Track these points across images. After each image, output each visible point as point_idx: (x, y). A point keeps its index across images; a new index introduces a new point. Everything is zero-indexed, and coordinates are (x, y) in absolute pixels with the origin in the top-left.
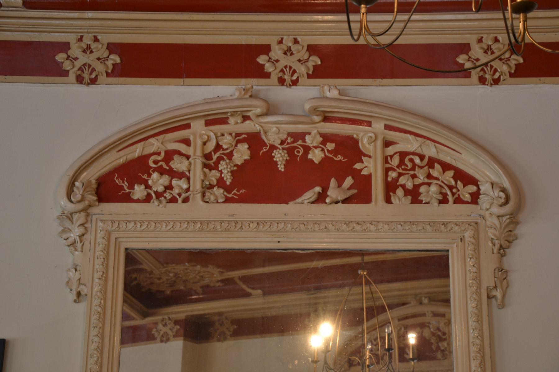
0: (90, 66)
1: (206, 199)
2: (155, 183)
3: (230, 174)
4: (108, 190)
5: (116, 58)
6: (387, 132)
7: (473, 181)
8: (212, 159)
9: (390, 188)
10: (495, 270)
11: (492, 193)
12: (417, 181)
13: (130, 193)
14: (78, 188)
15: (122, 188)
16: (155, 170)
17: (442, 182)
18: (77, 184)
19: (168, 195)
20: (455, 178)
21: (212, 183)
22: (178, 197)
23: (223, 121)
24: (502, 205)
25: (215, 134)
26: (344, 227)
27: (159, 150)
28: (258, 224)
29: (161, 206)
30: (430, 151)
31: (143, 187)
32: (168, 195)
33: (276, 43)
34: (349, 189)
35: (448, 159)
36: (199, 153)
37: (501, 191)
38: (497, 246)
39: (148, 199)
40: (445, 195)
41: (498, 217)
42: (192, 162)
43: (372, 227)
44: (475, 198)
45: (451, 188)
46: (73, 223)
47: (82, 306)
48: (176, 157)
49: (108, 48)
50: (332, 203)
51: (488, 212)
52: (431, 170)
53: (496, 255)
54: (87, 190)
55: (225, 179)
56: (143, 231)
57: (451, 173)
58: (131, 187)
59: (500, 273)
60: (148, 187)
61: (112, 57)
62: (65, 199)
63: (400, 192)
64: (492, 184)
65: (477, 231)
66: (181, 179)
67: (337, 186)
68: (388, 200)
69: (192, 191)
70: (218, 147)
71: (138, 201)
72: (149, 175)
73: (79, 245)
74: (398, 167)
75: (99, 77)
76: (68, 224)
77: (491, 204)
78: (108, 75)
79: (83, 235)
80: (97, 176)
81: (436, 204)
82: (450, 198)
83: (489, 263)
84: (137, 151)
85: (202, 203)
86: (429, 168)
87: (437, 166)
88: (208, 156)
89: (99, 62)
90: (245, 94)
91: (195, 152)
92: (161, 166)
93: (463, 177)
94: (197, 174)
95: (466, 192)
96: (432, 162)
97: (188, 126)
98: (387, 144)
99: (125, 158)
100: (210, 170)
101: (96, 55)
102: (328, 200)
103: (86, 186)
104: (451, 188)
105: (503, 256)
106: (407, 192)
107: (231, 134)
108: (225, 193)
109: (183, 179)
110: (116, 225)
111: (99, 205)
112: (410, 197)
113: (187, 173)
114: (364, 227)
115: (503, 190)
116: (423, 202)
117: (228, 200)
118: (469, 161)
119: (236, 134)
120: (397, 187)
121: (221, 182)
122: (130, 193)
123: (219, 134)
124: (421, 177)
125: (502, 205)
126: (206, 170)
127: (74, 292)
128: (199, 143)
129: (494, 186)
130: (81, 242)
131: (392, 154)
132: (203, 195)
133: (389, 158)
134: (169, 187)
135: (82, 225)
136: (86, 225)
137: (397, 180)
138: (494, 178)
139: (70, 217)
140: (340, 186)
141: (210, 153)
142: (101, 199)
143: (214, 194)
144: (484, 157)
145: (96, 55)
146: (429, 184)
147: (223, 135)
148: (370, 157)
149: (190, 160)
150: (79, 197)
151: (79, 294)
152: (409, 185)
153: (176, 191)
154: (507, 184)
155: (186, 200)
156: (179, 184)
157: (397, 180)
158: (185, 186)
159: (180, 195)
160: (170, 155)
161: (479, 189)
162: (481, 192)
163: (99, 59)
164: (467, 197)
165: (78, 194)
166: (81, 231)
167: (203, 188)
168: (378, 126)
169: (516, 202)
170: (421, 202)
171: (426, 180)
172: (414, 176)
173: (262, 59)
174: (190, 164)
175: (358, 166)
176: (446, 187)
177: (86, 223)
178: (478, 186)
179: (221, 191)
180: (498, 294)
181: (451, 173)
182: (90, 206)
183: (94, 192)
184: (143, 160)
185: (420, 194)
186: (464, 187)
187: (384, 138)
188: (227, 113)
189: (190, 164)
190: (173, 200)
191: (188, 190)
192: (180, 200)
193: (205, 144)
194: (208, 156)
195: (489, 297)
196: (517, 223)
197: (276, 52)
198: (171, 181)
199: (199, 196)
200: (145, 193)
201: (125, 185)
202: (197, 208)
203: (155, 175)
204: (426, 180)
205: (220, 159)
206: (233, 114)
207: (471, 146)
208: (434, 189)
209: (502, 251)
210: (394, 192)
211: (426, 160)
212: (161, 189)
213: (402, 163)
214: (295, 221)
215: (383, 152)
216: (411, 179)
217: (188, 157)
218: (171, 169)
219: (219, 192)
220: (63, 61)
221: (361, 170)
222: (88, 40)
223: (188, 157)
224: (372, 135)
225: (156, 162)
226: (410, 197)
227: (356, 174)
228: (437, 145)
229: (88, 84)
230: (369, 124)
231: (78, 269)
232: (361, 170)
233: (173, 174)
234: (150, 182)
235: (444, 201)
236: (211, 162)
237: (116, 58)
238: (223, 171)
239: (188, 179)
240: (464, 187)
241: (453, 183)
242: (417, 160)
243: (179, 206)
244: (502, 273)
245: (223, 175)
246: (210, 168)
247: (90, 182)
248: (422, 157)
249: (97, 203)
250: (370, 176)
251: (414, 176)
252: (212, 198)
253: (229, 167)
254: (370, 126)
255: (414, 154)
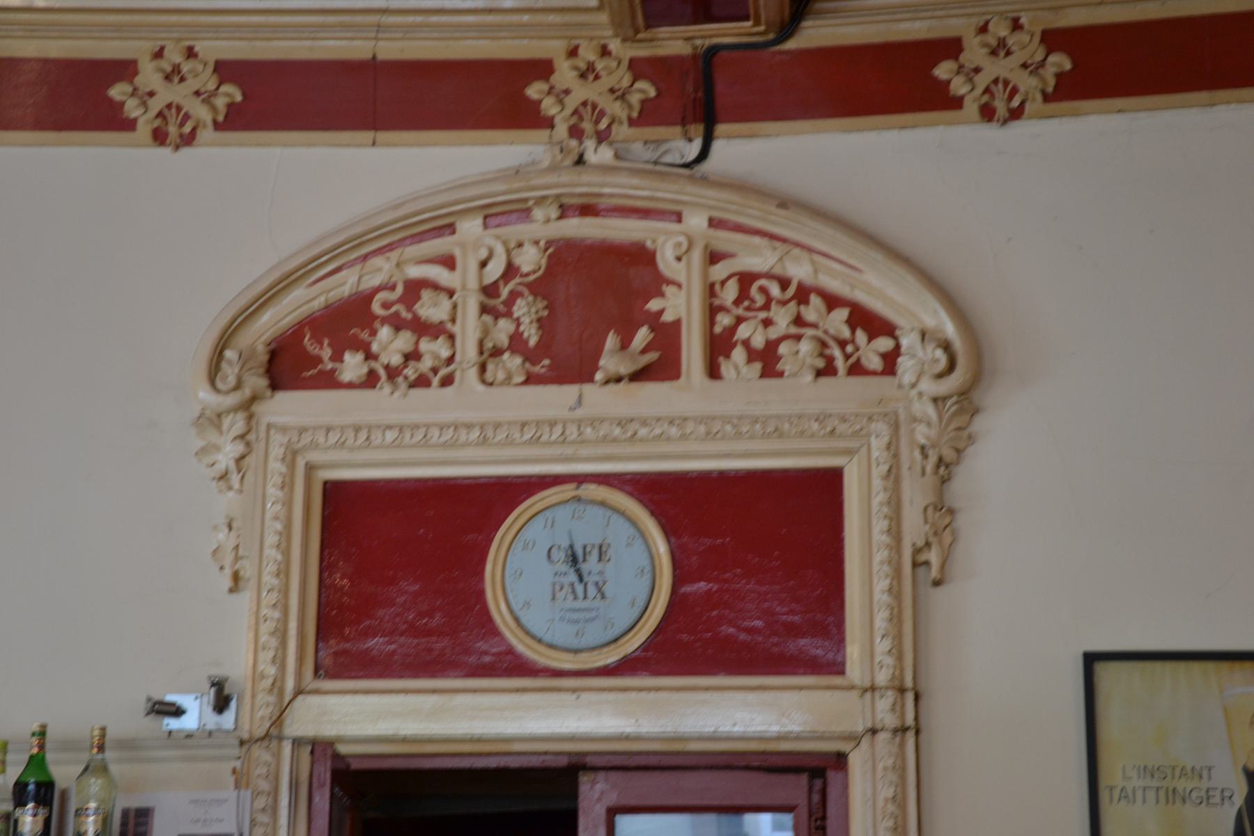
0: (1006, 83)
1: (489, 376)
2: (384, 348)
3: (535, 325)
4: (287, 365)
5: (1060, 62)
6: (712, 232)
7: (888, 329)
8: (498, 296)
9: (718, 347)
10: (925, 509)
11: (920, 354)
12: (773, 333)
13: (333, 371)
14: (230, 363)
15: (319, 360)
16: (384, 320)
17: (826, 332)
18: (229, 354)
19: (410, 372)
20: (852, 323)
21: (499, 344)
22: (431, 375)
23: (524, 213)
24: (940, 376)
25: (505, 243)
26: (816, 426)
27: (394, 279)
28: (401, 430)
29: (397, 394)
30: (799, 271)
31: (360, 357)
32: (410, 372)
33: (972, 32)
34: (644, 351)
35: (834, 285)
36: (473, 284)
37: (939, 346)
38: (933, 459)
39: (371, 381)
40: (830, 360)
41: (935, 400)
42: (460, 301)
43: (674, 431)
44: (890, 362)
45: (842, 344)
46: (221, 432)
47: (246, 598)
48: (426, 295)
49: (1043, 40)
50: (607, 382)
51: (914, 392)
52: (802, 308)
53: (930, 479)
54: (248, 366)
55: (526, 335)
56: (360, 448)
57: (842, 314)
58: (338, 357)
59: (938, 514)
60: (370, 356)
61: (225, 88)
62: (207, 386)
63: (739, 354)
64: (923, 335)
65: (896, 427)
66: (437, 338)
67: (618, 345)
68: (713, 372)
69: (461, 363)
70: (511, 271)
71: (350, 386)
72: (374, 333)
73: (235, 479)
74: (737, 302)
75: (198, 132)
76: (213, 436)
77: (920, 376)
78: (1047, 98)
79: (242, 457)
80: (268, 336)
81: (809, 377)
82: (840, 363)
83: (915, 496)
84: (346, 284)
85: (481, 388)
86: (799, 304)
87: (815, 300)
88: (490, 291)
89: (1026, 73)
90: (562, 160)
91: (466, 279)
92: (397, 314)
93: (868, 322)
94: (469, 327)
95: (871, 352)
96: (803, 294)
97: (451, 229)
98: (714, 257)
99: (322, 299)
100: (496, 318)
101: (192, 84)
102: (599, 376)
103: (245, 359)
104: (842, 344)
105: (944, 481)
106: (753, 355)
107: (537, 243)
108: (527, 365)
109: (441, 339)
110: (363, 436)
111: (272, 397)
112: (758, 366)
113: (449, 326)
114: (658, 431)
115: (947, 347)
116: (786, 374)
117: (530, 380)
118: (883, 289)
119: (547, 242)
120: (734, 345)
121: (516, 343)
122: (333, 371)
123: (512, 245)
124: (782, 319)
125: (940, 376)
126: (488, 318)
127: (228, 572)
128: (473, 266)
129: (927, 337)
130: (239, 471)
131: (724, 276)
132: (483, 368)
133: (717, 287)
134: (412, 356)
135: (242, 437)
136: (249, 437)
137: (732, 330)
138: (930, 322)
139: (214, 420)
140: (625, 345)
141: (496, 283)
142: (276, 385)
143: (504, 368)
144: (911, 280)
145: (192, 84)
146: (798, 338)
147: (520, 245)
148: (679, 286)
149: (455, 297)
150: (232, 380)
151: (236, 577)
152: (758, 342)
153: (426, 364)
154: (950, 329)
155: (447, 381)
156: (433, 349)
157: (732, 330)
158: (445, 353)
159: (435, 371)
160: (414, 289)
161: (898, 346)
162: (903, 349)
163: (1025, 66)
164: (875, 363)
165: (230, 372)
166: (240, 448)
167: (481, 353)
168: (696, 222)
169: (970, 373)
170: (781, 374)
171: (794, 330)
172: (767, 323)
173: (534, 91)
174: (455, 307)
175: (654, 305)
176: (832, 343)
177: (248, 432)
178: (896, 338)
179: (518, 360)
180: (933, 557)
181: (842, 314)
182: (254, 399)
183: (262, 370)
184: (364, 299)
185: (779, 358)
186: (870, 340)
187: (706, 247)
188: (526, 200)
189: (455, 307)
190: (422, 382)
191: (450, 360)
192: (436, 381)
193: (484, 264)
194: (490, 291)
195: (915, 565)
196: (975, 412)
197: (149, 76)
198: (417, 343)
199: (473, 373)
200: (365, 370)
201: (326, 353)
202: (468, 400)
203: (385, 332)
204: (794, 330)
205: (514, 295)
206: (540, 201)
207: (877, 256)
208: (806, 347)
209: (945, 469)
210: (728, 356)
211: (791, 291)
212: (396, 360)
213: (743, 295)
214: (714, 418)
215: (705, 275)
216: (760, 328)
217: (451, 293)
218: (416, 318)
219: (513, 362)
220: (124, 98)
221: (661, 312)
222: (174, 55)
223: (451, 293)
224: (682, 239)
225: (386, 305)
226: (758, 366)
227: (654, 319)
228: (816, 257)
229: (1005, 122)
230: (679, 218)
231: (235, 525)
232: (661, 312)
233: (423, 329)
234: (375, 347)
235: (827, 370)
236: (497, 303)
237: (1060, 62)
238: (522, 320)
239: (452, 337)
240: (870, 340)
241: (846, 333)
242: (775, 290)
243: (434, 393)
244: (943, 511)
245: (522, 328)
246: (497, 316)
247: (253, 349)
248: (784, 283)
249: (269, 393)
250: (677, 324)
251: (767, 323)
252: (501, 376)
253: (533, 310)
254: (679, 220)
255: (769, 276)
